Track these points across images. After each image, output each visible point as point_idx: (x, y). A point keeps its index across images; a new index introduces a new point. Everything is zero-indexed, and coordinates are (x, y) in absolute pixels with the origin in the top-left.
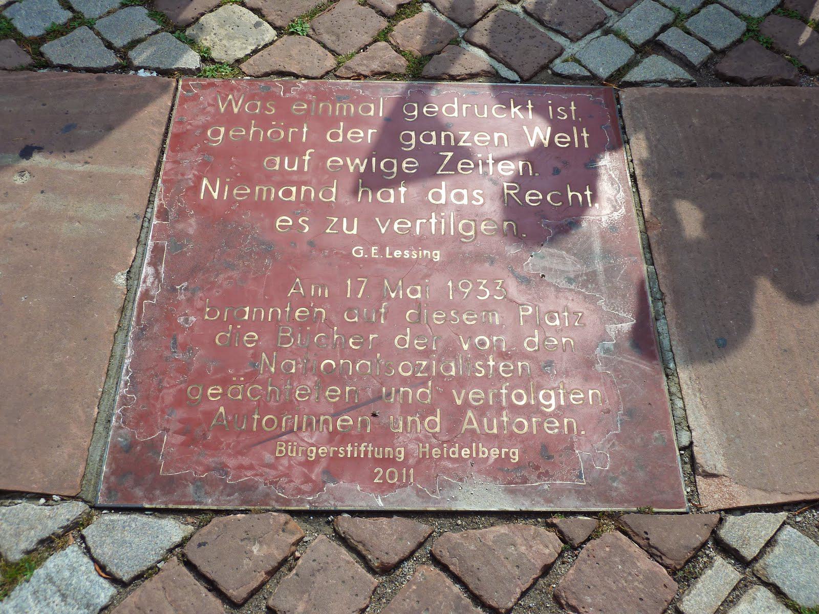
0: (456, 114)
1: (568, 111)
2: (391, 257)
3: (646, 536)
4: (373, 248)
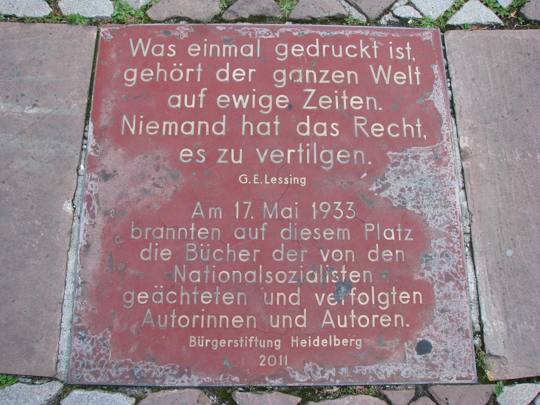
0: (317, 54)
1: (405, 51)
2: (269, 183)
3: (446, 401)
4: (255, 175)
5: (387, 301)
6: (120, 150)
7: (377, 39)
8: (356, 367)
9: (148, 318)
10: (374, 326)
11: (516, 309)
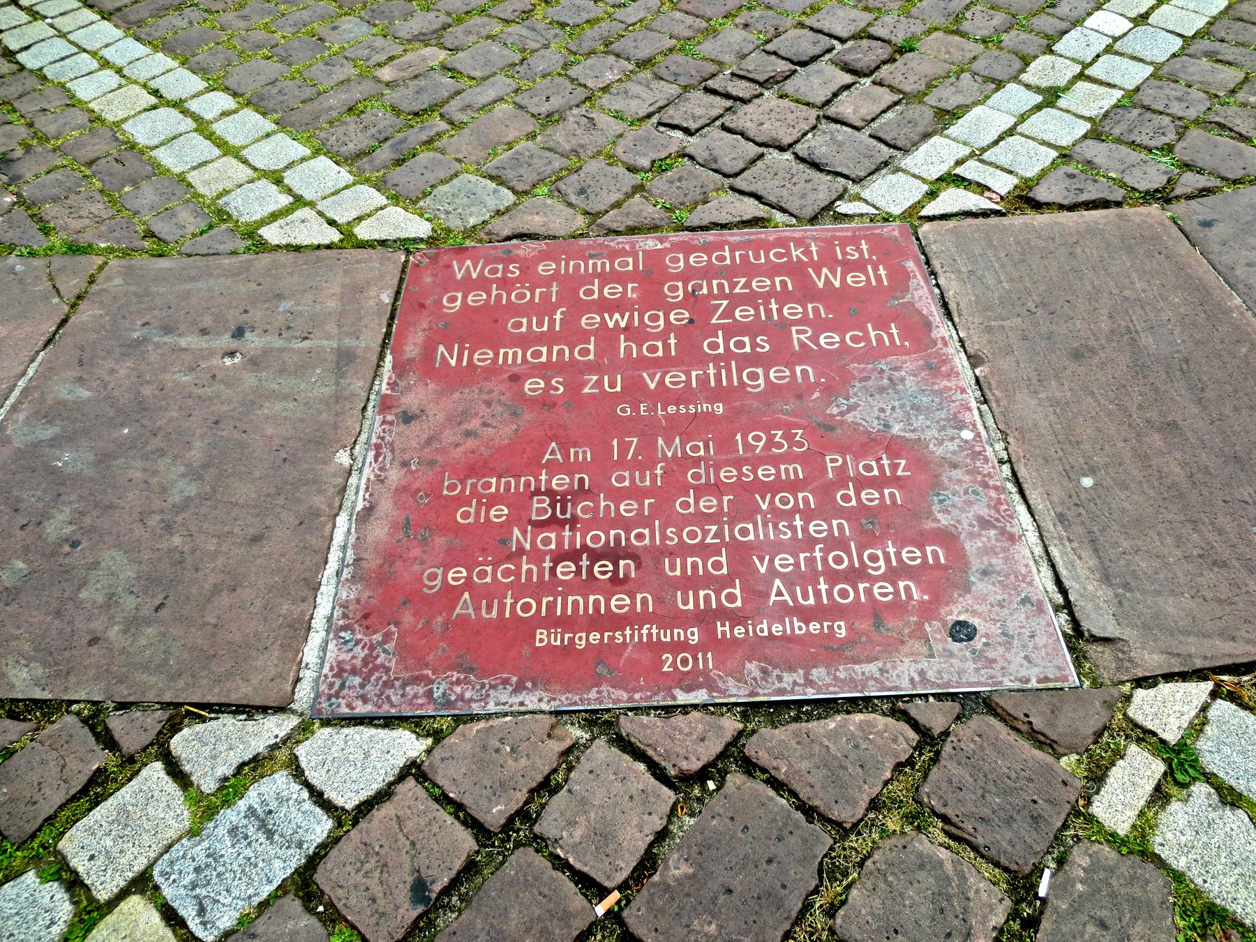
5: (882, 562)
6: (432, 386)
7: (815, 239)
8: (841, 668)
9: (464, 606)
10: (863, 600)
11: (1122, 562)
